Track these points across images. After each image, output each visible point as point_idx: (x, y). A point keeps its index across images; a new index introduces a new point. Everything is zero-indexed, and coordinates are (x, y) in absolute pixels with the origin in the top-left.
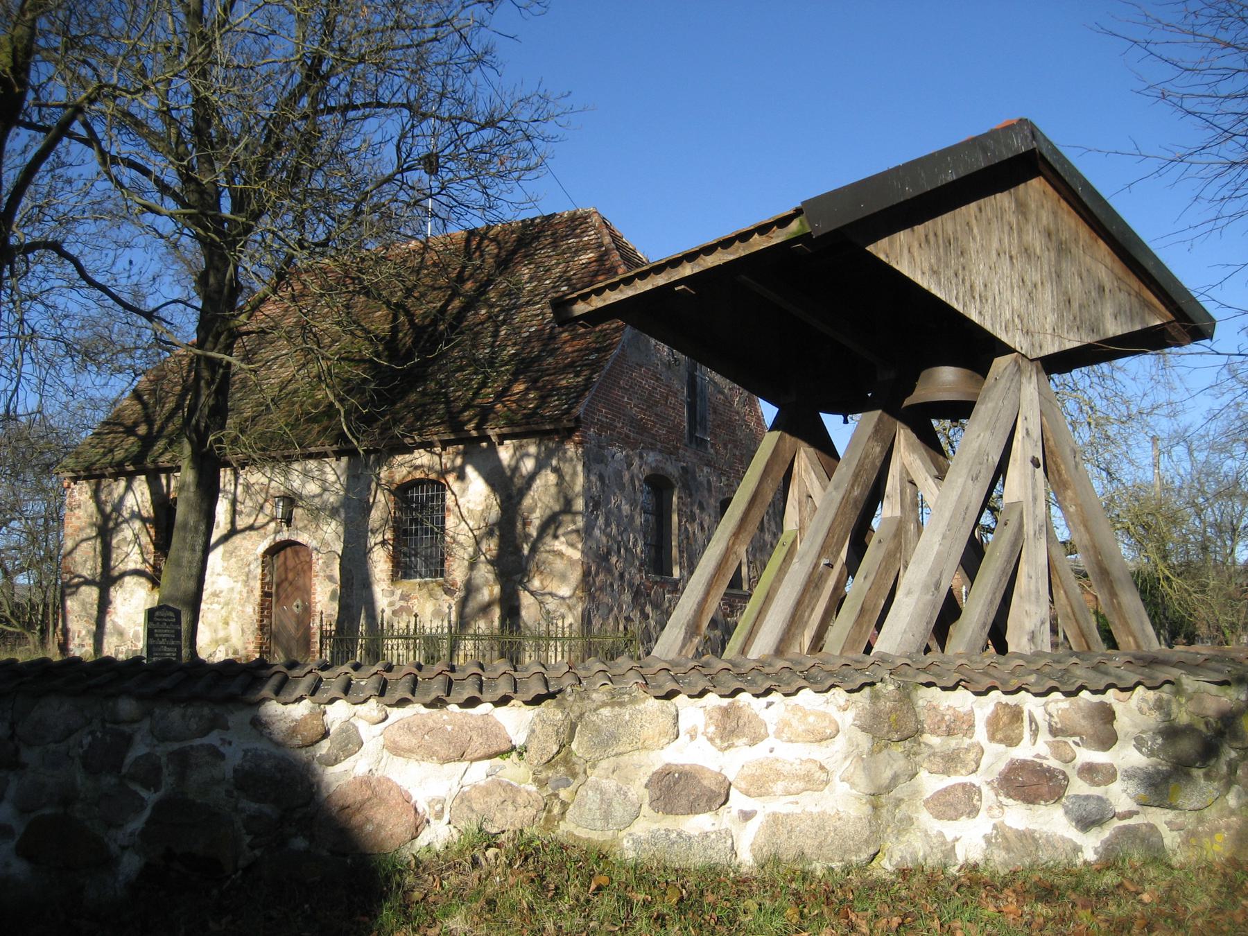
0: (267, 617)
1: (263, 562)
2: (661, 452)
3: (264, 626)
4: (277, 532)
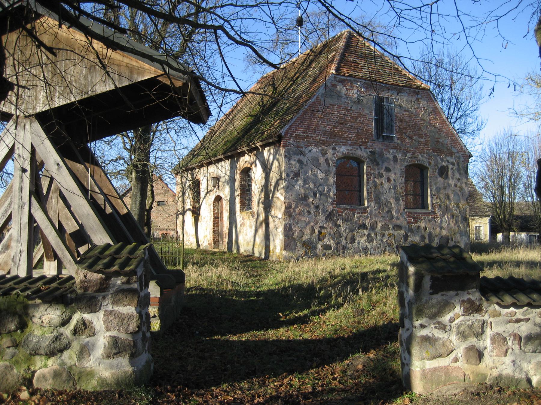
0: (217, 227)
1: (214, 205)
2: (350, 145)
3: (216, 230)
4: (216, 192)
